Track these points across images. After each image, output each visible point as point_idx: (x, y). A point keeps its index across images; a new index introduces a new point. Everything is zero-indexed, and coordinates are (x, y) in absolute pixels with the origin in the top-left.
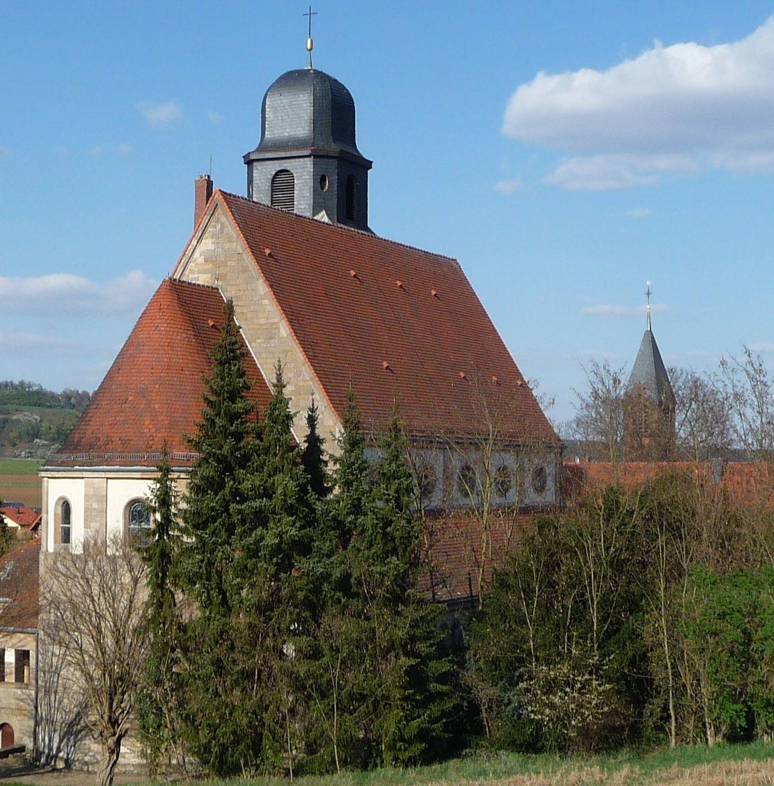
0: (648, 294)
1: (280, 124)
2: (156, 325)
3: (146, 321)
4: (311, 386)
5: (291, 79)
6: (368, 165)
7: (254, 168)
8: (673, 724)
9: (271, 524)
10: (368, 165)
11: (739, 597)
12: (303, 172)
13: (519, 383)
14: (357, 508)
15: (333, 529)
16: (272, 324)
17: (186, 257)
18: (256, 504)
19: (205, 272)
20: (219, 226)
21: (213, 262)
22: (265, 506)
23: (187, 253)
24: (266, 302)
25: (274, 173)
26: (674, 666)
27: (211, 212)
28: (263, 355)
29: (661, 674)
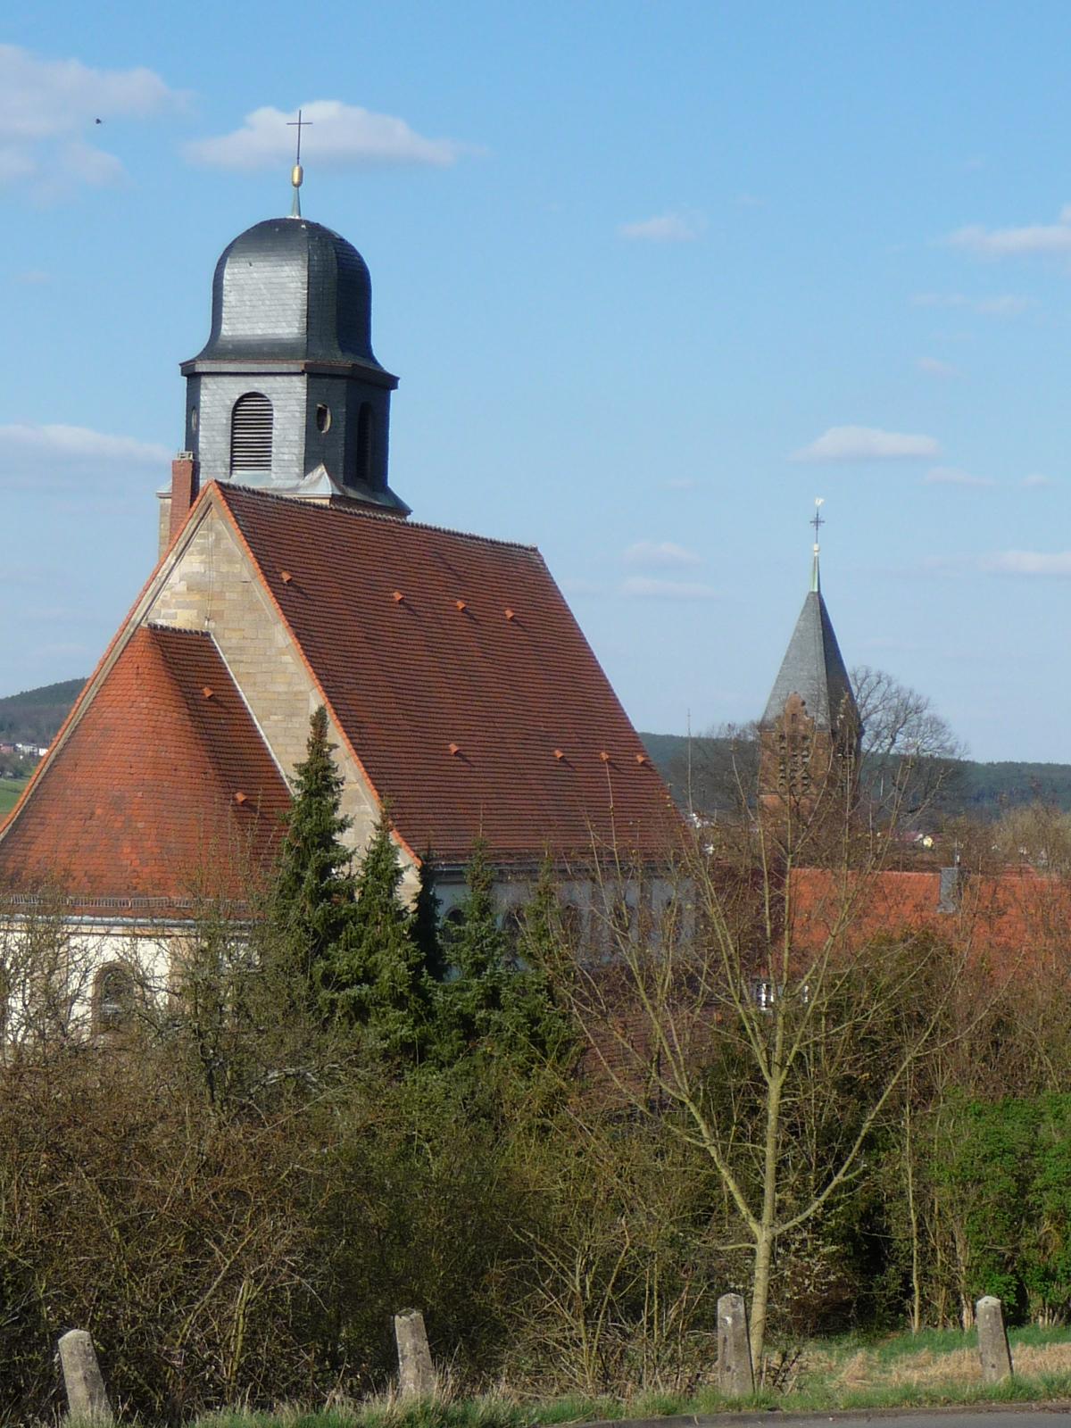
0: (817, 522)
1: (247, 314)
2: (132, 698)
3: (114, 692)
4: (357, 790)
5: (269, 236)
6: (390, 382)
7: (202, 386)
8: (917, 1300)
9: (372, 1020)
10: (390, 382)
11: (1015, 1133)
12: (288, 400)
13: (640, 759)
14: (492, 999)
15: (457, 1026)
16: (296, 694)
17: (156, 582)
18: (353, 991)
19: (188, 606)
20: (212, 537)
21: (200, 591)
22: (366, 995)
23: (159, 575)
24: (288, 658)
25: (237, 397)
26: (920, 1224)
27: (201, 515)
28: (281, 740)
29: (903, 1229)
